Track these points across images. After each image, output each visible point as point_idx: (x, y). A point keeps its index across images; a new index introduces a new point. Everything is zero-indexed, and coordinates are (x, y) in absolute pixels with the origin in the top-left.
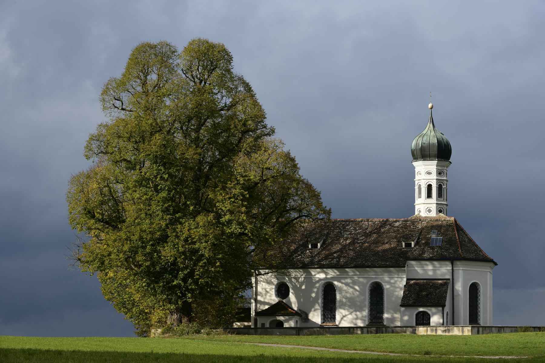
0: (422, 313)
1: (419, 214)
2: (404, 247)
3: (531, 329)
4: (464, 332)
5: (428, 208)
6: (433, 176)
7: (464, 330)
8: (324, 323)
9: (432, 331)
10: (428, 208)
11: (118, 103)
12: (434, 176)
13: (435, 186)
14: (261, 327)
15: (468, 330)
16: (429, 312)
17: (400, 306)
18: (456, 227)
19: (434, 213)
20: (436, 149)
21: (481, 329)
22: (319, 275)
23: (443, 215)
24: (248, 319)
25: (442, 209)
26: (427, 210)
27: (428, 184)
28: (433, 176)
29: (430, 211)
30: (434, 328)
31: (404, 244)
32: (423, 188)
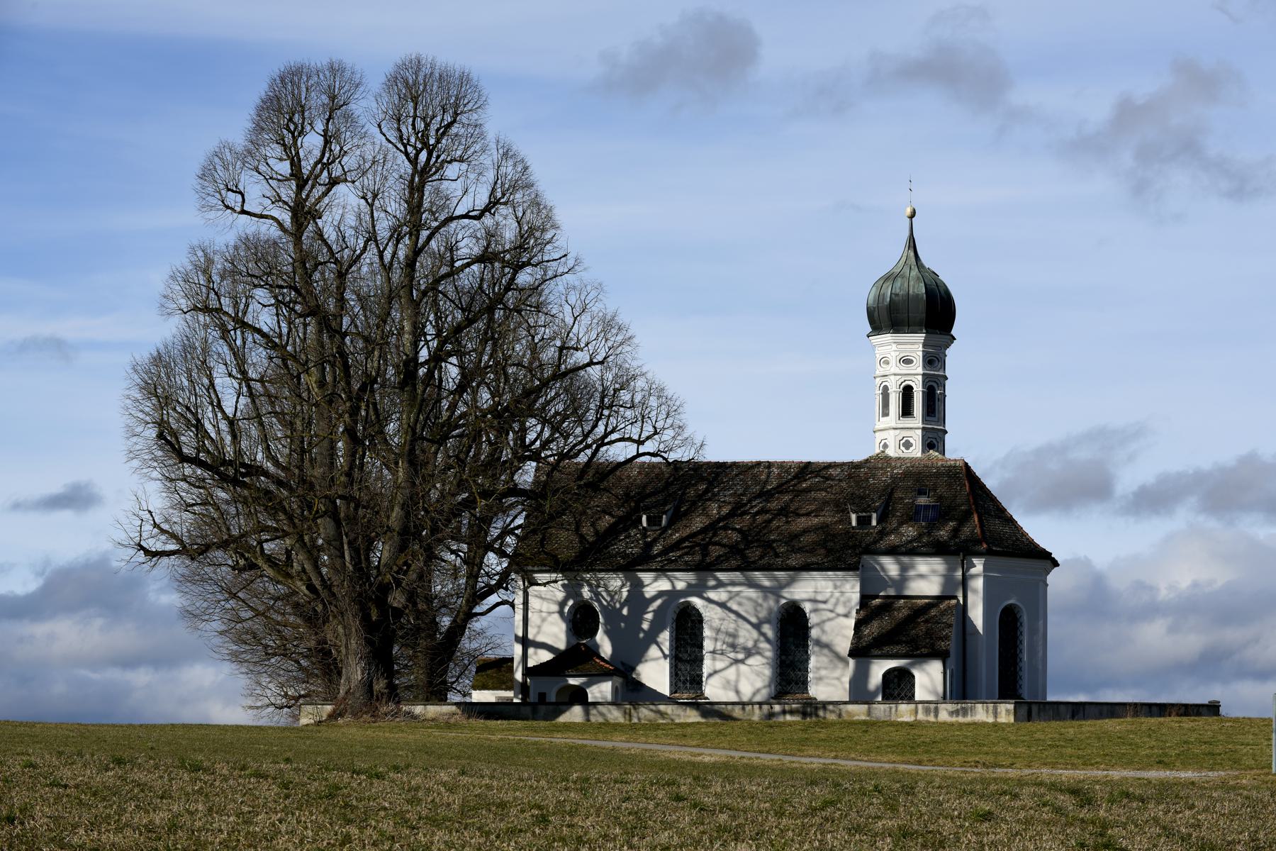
0: (896, 673)
1: (883, 452)
2: (854, 523)
3: (1145, 709)
4: (998, 716)
5: (905, 439)
6: (915, 367)
8: (676, 692)
9: (927, 711)
10: (905, 439)
11: (233, 199)
12: (918, 368)
13: (921, 389)
14: (537, 701)
15: (1007, 711)
16: (797, 597)
19: (917, 450)
20: (922, 307)
21: (1035, 709)
22: (654, 585)
23: (937, 454)
24: (507, 683)
25: (934, 441)
26: (902, 442)
27: (904, 384)
28: (915, 367)
29: (908, 445)
30: (932, 706)
31: (854, 517)
32: (894, 394)
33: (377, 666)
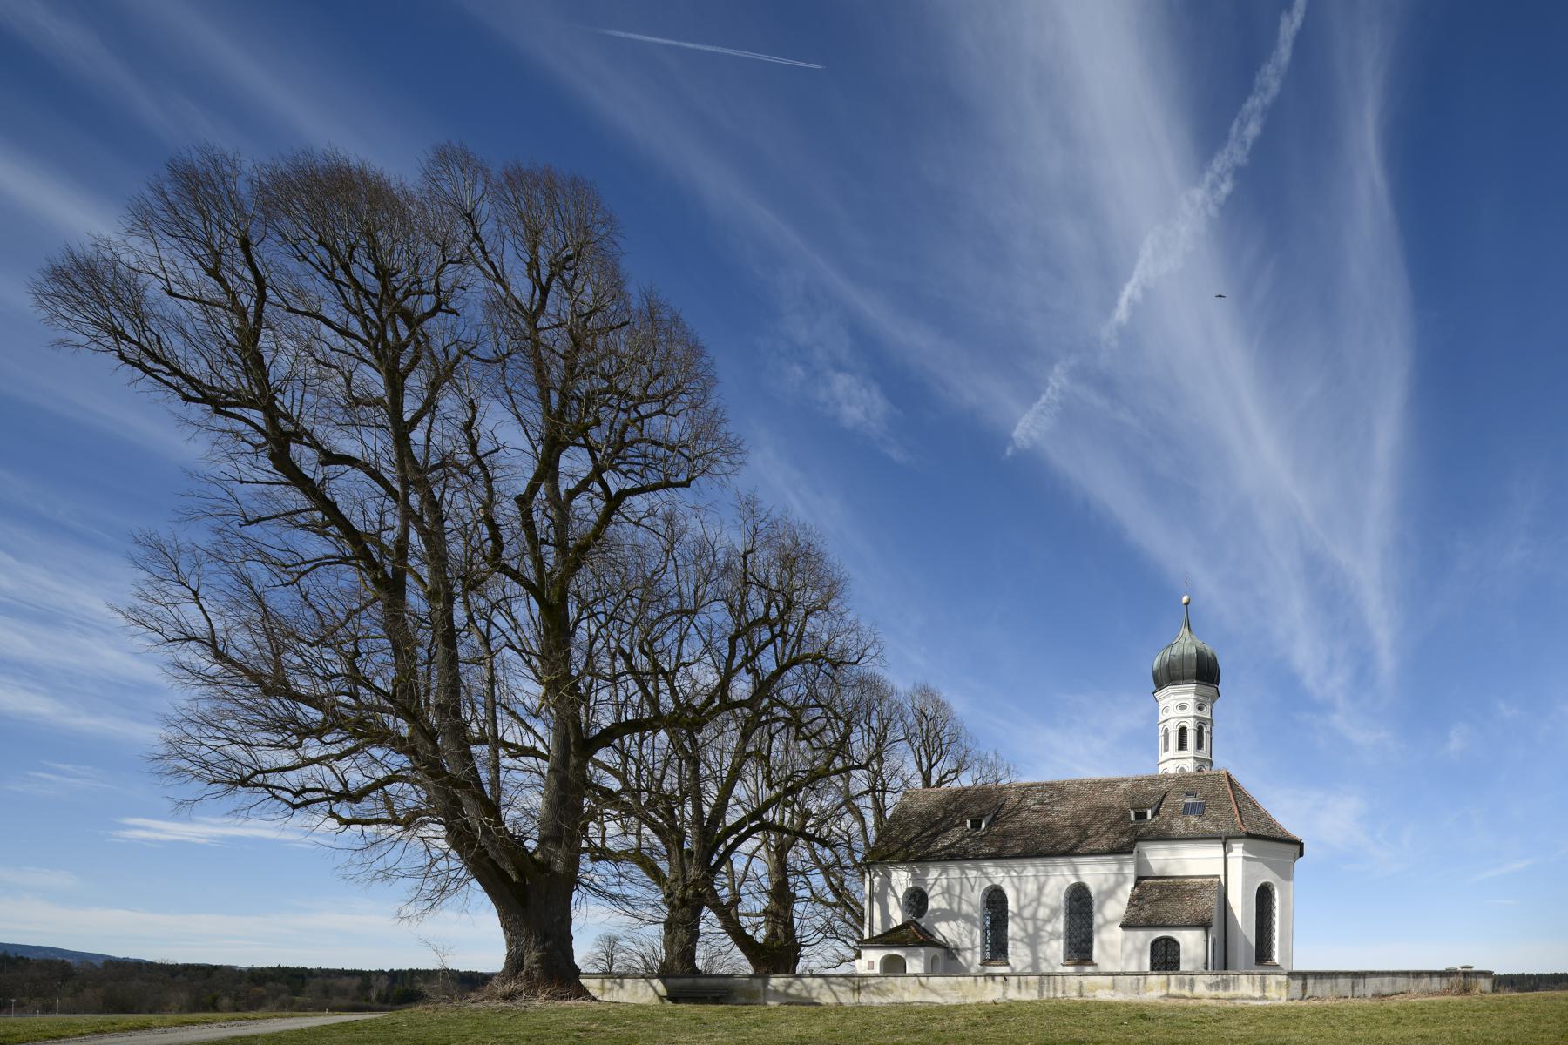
7: (1267, 983)
9: (1181, 984)
12: (1191, 710)
15: (1278, 984)
16: (1179, 939)
17: (58, 275)
18: (1231, 784)
20: (1194, 663)
30: (1187, 978)
33: (527, 937)
